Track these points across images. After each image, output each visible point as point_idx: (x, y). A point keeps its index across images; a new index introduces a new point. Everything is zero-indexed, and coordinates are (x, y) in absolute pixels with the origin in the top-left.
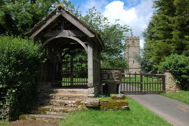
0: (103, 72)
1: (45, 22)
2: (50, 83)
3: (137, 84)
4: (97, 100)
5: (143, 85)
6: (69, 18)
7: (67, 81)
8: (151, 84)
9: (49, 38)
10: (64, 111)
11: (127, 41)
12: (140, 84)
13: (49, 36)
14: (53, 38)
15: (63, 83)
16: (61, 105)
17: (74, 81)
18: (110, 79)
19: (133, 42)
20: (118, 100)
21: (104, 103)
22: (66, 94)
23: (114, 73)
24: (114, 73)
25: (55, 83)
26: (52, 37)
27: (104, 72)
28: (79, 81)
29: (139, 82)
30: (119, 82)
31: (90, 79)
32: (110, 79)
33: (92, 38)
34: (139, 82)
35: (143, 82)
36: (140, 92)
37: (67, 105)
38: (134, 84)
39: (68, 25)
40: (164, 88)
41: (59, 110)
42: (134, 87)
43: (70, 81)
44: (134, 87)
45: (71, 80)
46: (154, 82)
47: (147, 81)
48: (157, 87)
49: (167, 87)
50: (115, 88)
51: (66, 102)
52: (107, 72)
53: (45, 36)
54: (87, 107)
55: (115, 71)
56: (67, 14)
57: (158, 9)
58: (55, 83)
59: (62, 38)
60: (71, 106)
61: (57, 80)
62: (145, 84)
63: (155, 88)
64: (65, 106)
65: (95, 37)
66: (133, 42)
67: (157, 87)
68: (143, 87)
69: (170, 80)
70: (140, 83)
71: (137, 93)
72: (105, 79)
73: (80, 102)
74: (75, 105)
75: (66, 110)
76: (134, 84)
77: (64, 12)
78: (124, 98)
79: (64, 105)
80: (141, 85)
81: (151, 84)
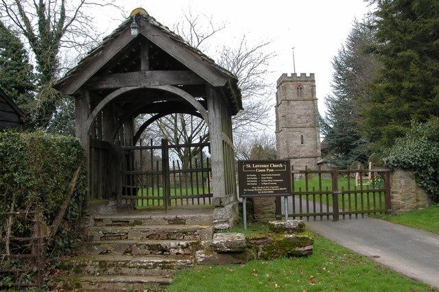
0: (245, 168)
1: (101, 52)
2: (112, 203)
3: (324, 196)
4: (239, 237)
5: (340, 197)
6: (161, 42)
7: (150, 195)
8: (359, 195)
9: (112, 90)
10: (164, 266)
11: (283, 85)
12: (330, 196)
13: (112, 86)
14: (123, 90)
15: (140, 201)
16: (151, 253)
17: (172, 194)
18: (264, 186)
19: (300, 88)
20: (289, 233)
21: (258, 242)
22: (161, 227)
23: (273, 170)
24: (273, 170)
25: (124, 202)
26: (119, 88)
27: (249, 169)
28: (206, 198)
29: (330, 189)
30: (284, 191)
31: (217, 186)
32: (264, 186)
33: (219, 87)
34: (330, 189)
35: (339, 188)
36: (331, 214)
37: (166, 251)
38: (317, 196)
39: (157, 53)
40: (388, 203)
41: (152, 264)
42: (311, 203)
43: (161, 195)
44: (311, 203)
45: (165, 191)
46: (365, 189)
47: (141, 153)
48: (365, 201)
49: (397, 199)
50: (273, 208)
51: (164, 243)
52: (255, 169)
53: (101, 87)
54: (220, 253)
55: (274, 166)
56: (154, 32)
57: (378, 18)
58: (124, 202)
59: (145, 90)
60: (178, 254)
61: (129, 194)
62: (343, 194)
63: (350, 201)
64: (162, 254)
65: (227, 84)
66: (300, 88)
67: (365, 201)
68: (340, 203)
69: (403, 187)
70: (331, 193)
71: (325, 217)
72: (250, 187)
73: (198, 243)
74: (187, 251)
75: (170, 263)
76: (317, 196)
77: (148, 28)
78: (301, 228)
79: (160, 252)
80: (335, 196)
81: (359, 195)
